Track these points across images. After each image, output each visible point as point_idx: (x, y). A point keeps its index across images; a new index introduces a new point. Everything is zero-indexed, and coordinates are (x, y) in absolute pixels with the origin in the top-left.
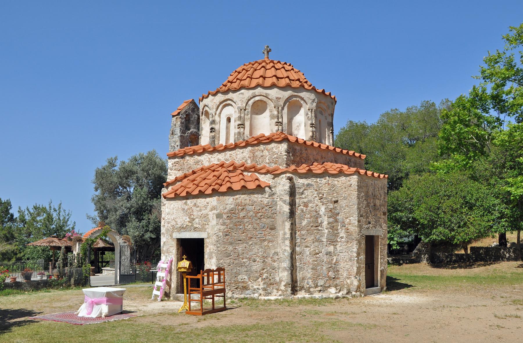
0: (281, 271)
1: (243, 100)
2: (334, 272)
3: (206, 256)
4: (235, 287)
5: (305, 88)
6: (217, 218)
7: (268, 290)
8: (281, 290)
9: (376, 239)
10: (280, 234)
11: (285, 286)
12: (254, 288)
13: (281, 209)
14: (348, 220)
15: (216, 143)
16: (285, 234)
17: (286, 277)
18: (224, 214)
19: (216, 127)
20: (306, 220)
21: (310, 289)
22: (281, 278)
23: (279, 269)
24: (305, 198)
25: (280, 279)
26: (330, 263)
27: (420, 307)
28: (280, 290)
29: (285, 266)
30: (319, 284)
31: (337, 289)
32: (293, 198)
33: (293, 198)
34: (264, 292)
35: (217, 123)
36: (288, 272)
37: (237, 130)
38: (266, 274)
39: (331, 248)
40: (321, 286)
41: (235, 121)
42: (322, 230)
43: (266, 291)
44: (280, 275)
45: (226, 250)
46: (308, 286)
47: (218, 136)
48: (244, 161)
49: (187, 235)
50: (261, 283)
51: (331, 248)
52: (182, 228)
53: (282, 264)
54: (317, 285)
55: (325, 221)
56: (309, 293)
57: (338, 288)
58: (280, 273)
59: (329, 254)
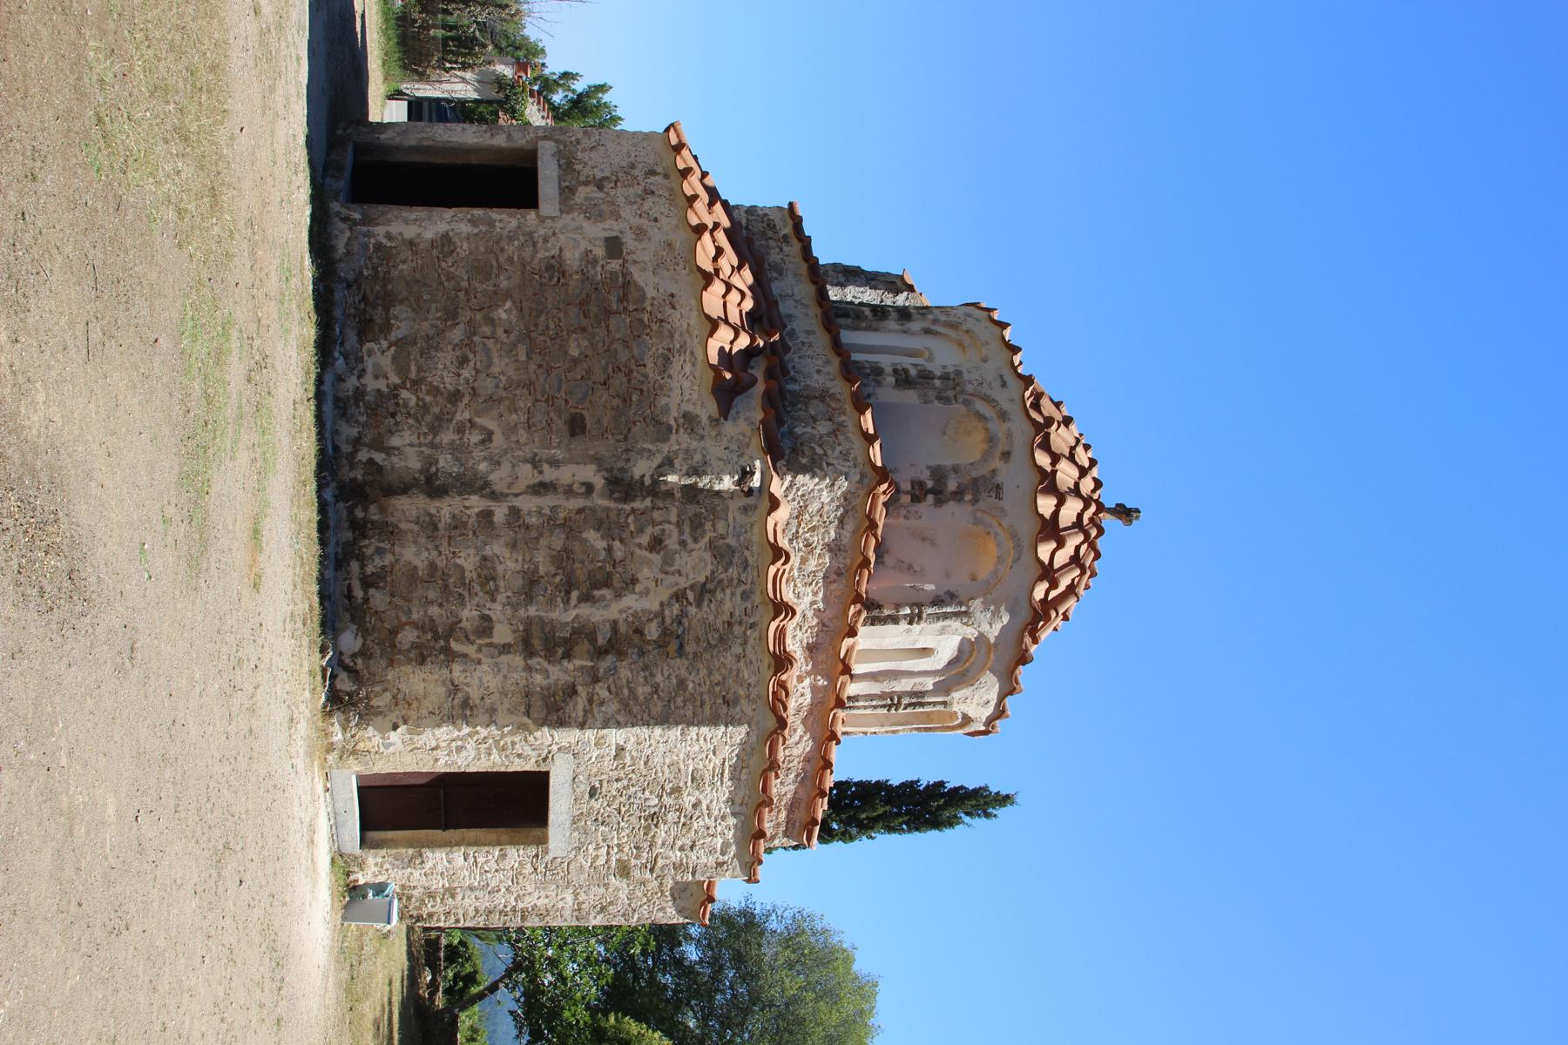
0: (423, 452)
1: (985, 385)
2: (415, 646)
3: (478, 212)
4: (368, 292)
5: (1007, 695)
6: (607, 239)
7: (358, 407)
8: (356, 451)
9: (536, 832)
10: (553, 451)
11: (371, 461)
12: (366, 358)
13: (640, 452)
14: (604, 694)
15: (842, 321)
16: (555, 463)
17: (403, 464)
18: (621, 261)
19: (891, 324)
20: (604, 544)
21: (357, 560)
22: (396, 452)
23: (433, 446)
24: (683, 543)
25: (394, 448)
26: (452, 629)
27: (278, 956)
28: (354, 447)
29: (441, 463)
30: (372, 591)
31: (354, 656)
32: (678, 495)
33: (678, 495)
34: (350, 393)
35: (902, 325)
36: (421, 472)
37: (889, 370)
38: (413, 401)
39: (503, 634)
40: (366, 600)
41: (915, 365)
42: (567, 601)
43: (352, 402)
44: (409, 450)
45: (500, 267)
46: (369, 551)
47: (864, 325)
48: (792, 373)
49: (548, 173)
50: (381, 385)
51: (503, 634)
52: (567, 163)
53: (449, 456)
54: (371, 585)
55: (606, 612)
56: (340, 557)
57: (359, 661)
58: (416, 449)
59: (485, 626)
